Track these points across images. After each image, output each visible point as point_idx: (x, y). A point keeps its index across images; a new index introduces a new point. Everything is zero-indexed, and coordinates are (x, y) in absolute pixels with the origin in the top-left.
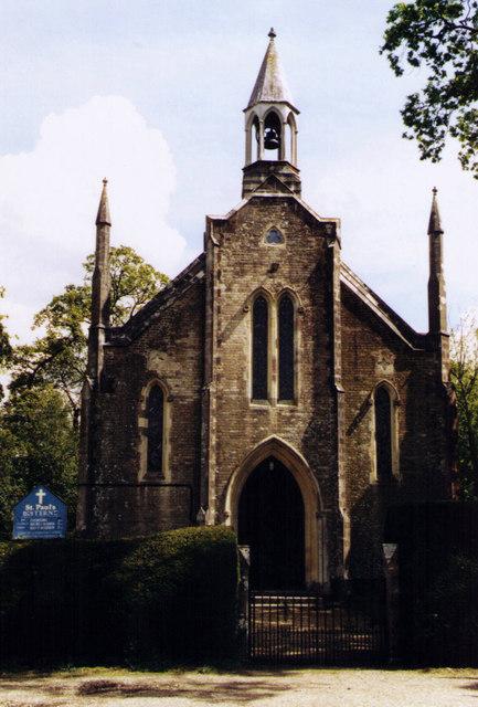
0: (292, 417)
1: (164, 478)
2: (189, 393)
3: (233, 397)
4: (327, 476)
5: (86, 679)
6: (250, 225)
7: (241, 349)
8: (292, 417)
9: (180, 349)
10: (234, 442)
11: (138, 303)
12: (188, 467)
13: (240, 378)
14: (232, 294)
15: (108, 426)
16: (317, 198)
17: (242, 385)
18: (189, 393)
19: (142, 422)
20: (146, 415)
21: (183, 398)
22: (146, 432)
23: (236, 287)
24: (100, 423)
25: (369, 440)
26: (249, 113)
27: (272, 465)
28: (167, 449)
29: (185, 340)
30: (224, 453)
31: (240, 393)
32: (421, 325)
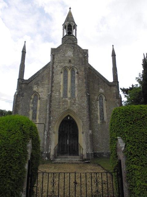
0: (74, 103)
1: (36, 122)
2: (45, 97)
3: (57, 97)
4: (85, 121)
5: (61, 93)
6: (63, 50)
7: (60, 83)
8: (74, 103)
9: (43, 85)
10: (57, 110)
11: (40, 98)
12: (116, 176)
13: (59, 91)
14: (58, 68)
15: (21, 106)
16: (82, 43)
17: (60, 94)
18: (45, 97)
19: (31, 105)
20: (33, 103)
21: (43, 98)
22: (33, 108)
23: (58, 66)
24: (19, 105)
25: (98, 111)
26: (64, 25)
27: (69, 118)
28: (38, 113)
29: (44, 82)
30: (54, 113)
31: (59, 96)
32: (110, 79)
